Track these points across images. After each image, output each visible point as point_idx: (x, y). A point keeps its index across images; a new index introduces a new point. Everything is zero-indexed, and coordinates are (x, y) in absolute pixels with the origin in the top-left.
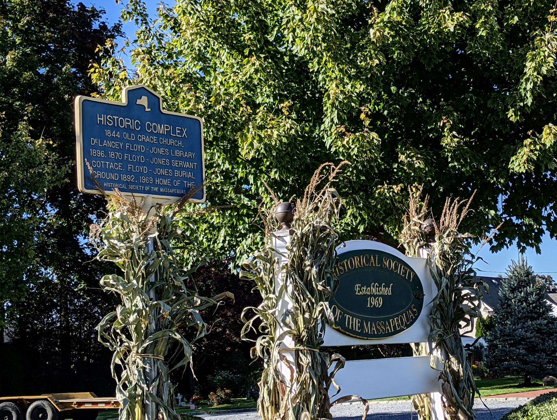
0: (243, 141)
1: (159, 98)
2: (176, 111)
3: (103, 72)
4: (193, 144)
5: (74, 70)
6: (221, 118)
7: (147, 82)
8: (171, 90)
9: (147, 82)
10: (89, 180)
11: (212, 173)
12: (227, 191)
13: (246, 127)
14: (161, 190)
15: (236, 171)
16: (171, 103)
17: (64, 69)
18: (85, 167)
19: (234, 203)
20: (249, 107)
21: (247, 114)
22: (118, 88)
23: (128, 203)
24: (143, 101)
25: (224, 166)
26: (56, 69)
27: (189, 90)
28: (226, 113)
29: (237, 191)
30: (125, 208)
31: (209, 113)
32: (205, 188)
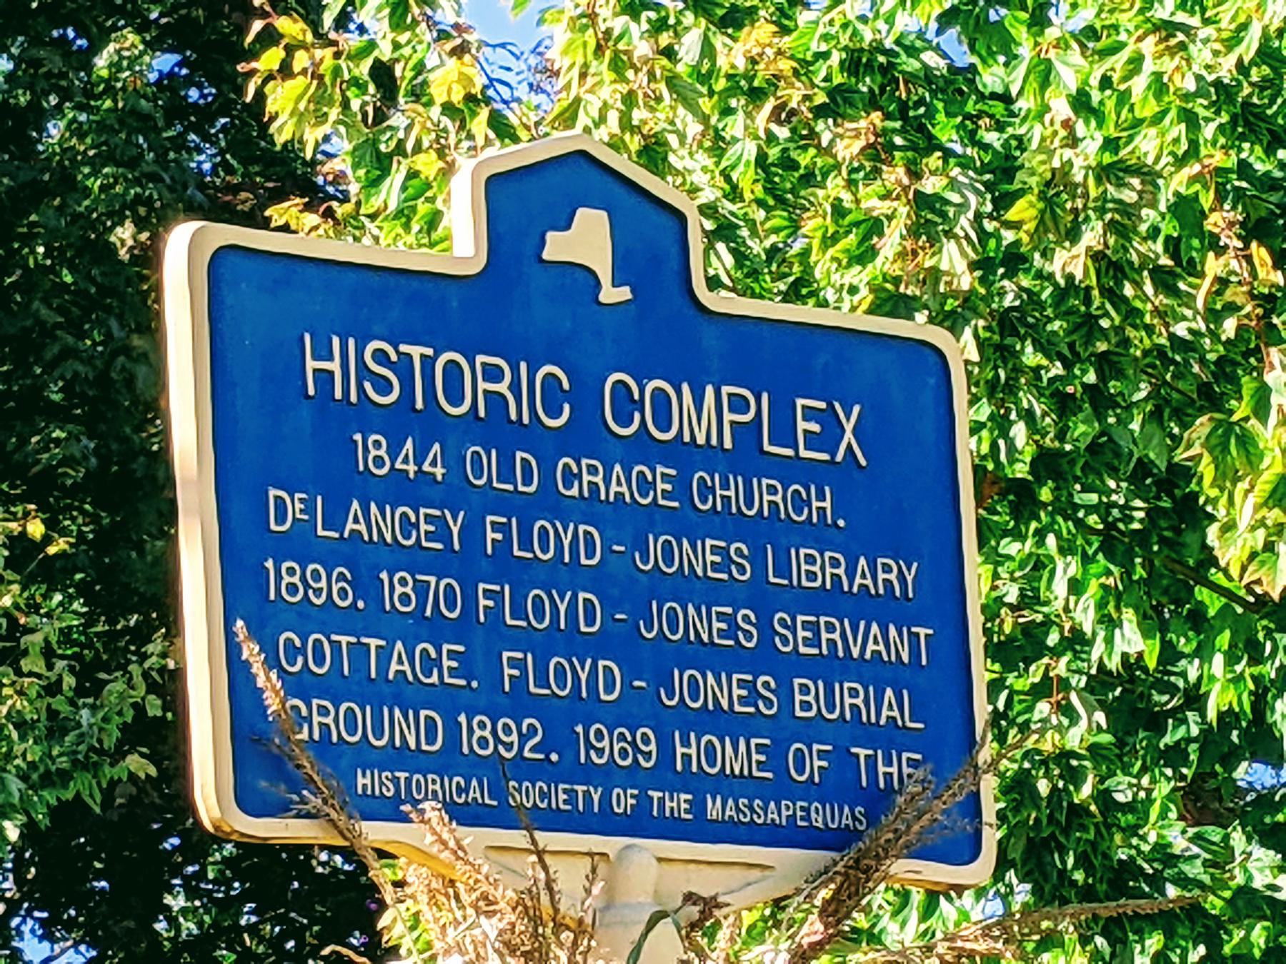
0: (1227, 477)
1: (681, 218)
2: (794, 294)
3: (337, 71)
4: (901, 500)
5: (165, 61)
6: (1087, 325)
7: (602, 119)
8: (761, 160)
9: (602, 119)
10: (263, 761)
11: (1040, 691)
12: (1138, 808)
13: (1248, 385)
14: (714, 809)
15: (1193, 675)
16: (757, 248)
17: (101, 63)
18: (237, 670)
19: (1183, 881)
20: (1260, 253)
21: (1252, 296)
22: (428, 164)
23: (505, 895)
24: (586, 240)
25: (1109, 641)
26: (55, 63)
27: (879, 153)
28: (1113, 295)
29: (1204, 802)
30: (491, 927)
31: (1008, 301)
32: (989, 786)
